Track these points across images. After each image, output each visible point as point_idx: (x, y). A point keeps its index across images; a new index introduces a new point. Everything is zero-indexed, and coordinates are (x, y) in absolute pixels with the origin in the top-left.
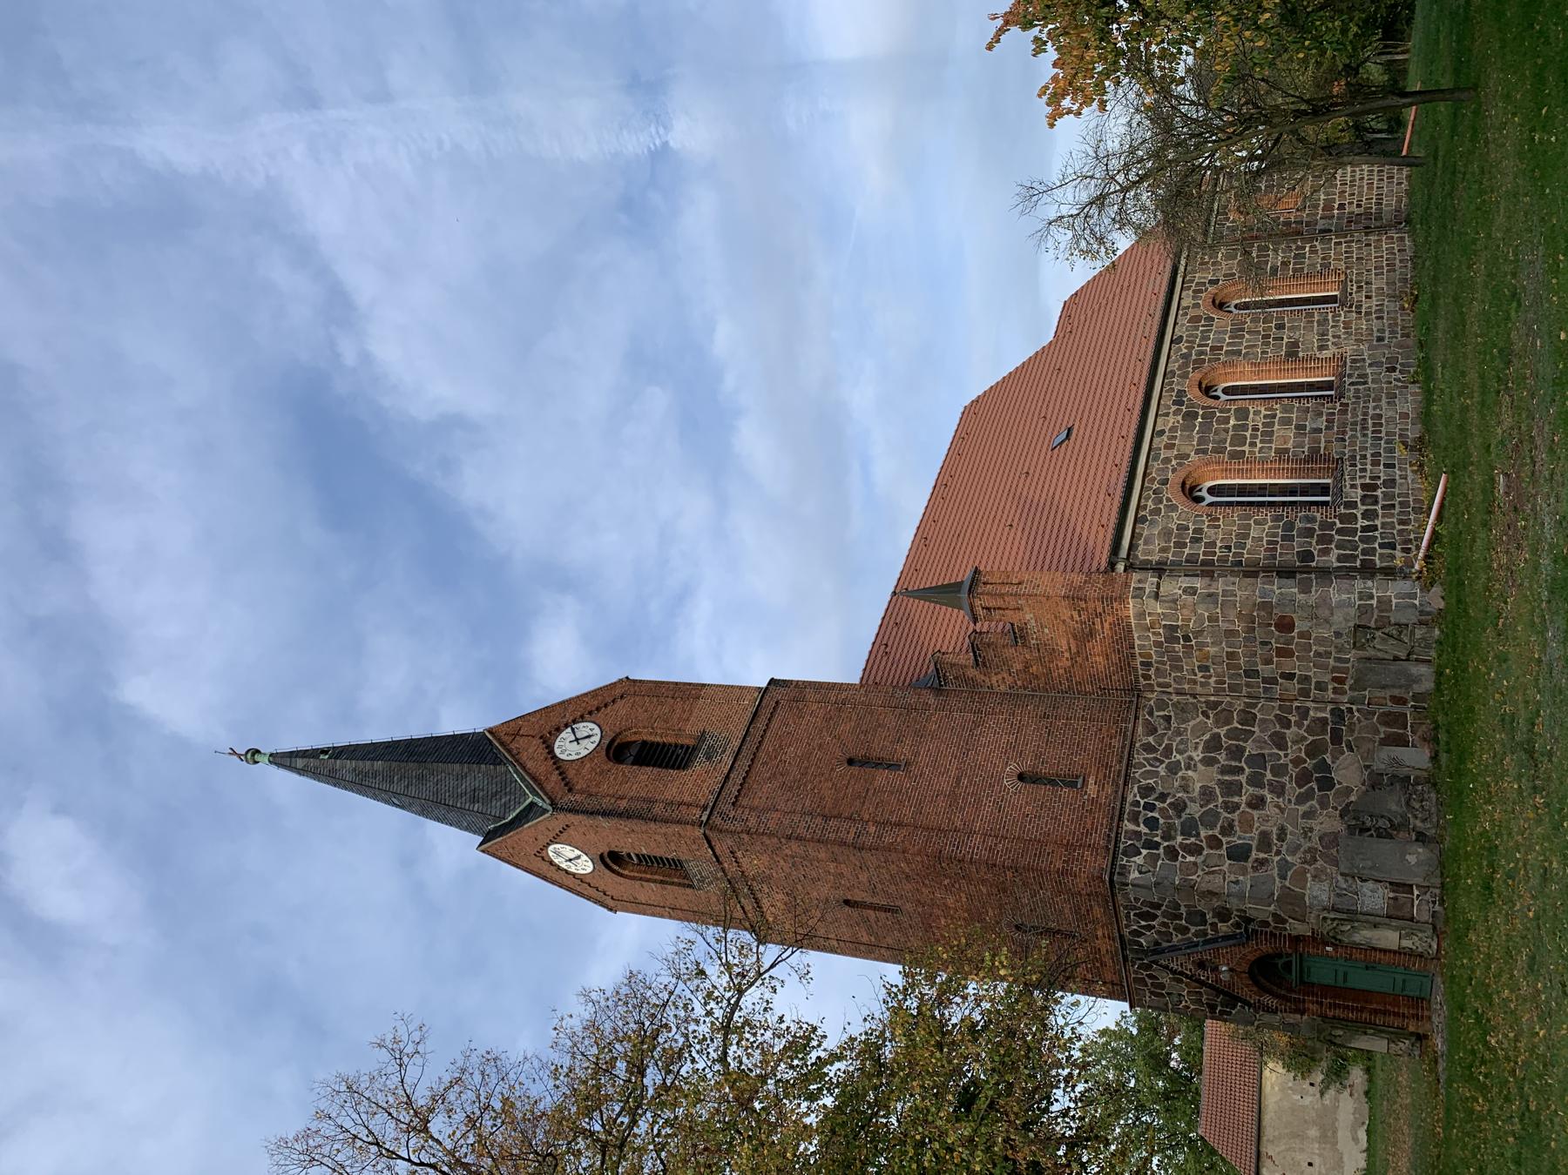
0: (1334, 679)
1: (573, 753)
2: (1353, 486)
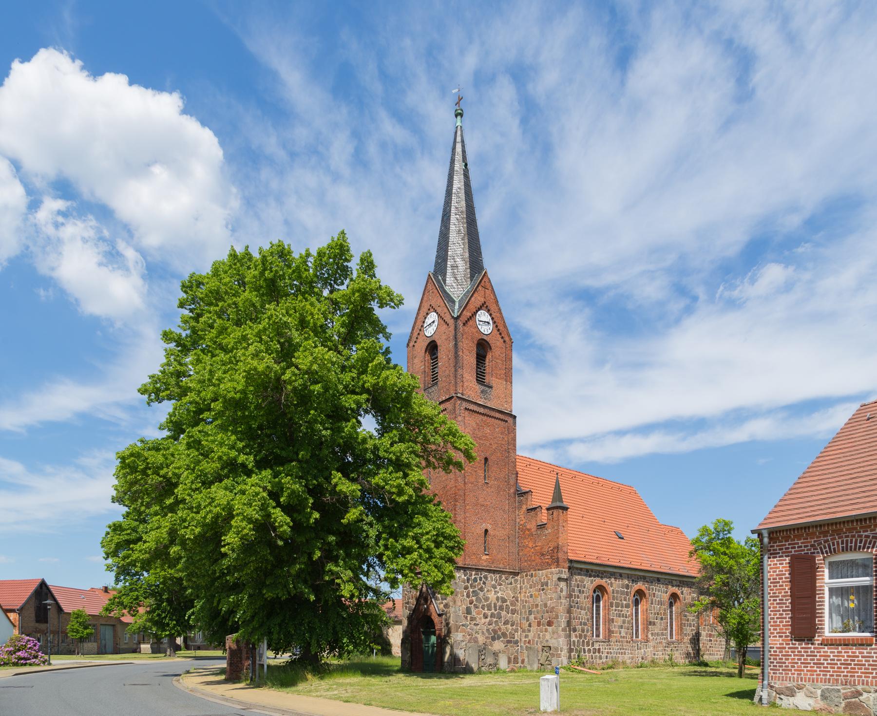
0: (530, 641)
2: (600, 645)
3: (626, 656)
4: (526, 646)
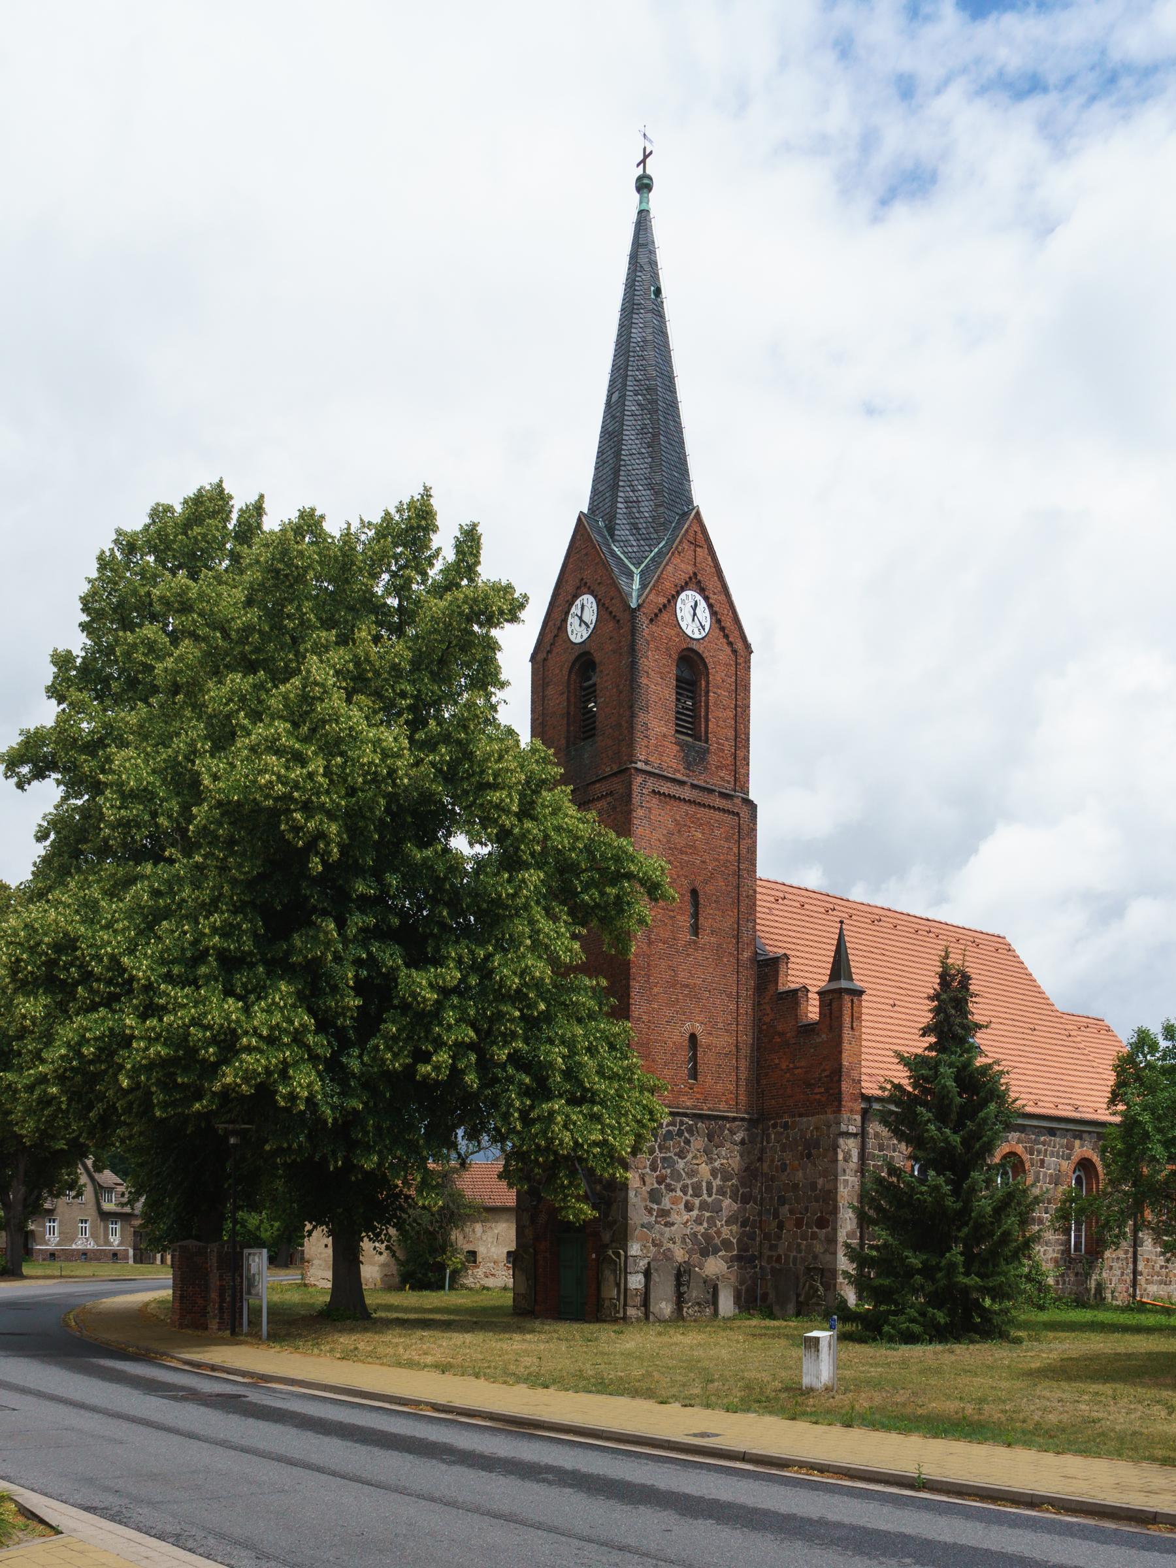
1: (682, 614)
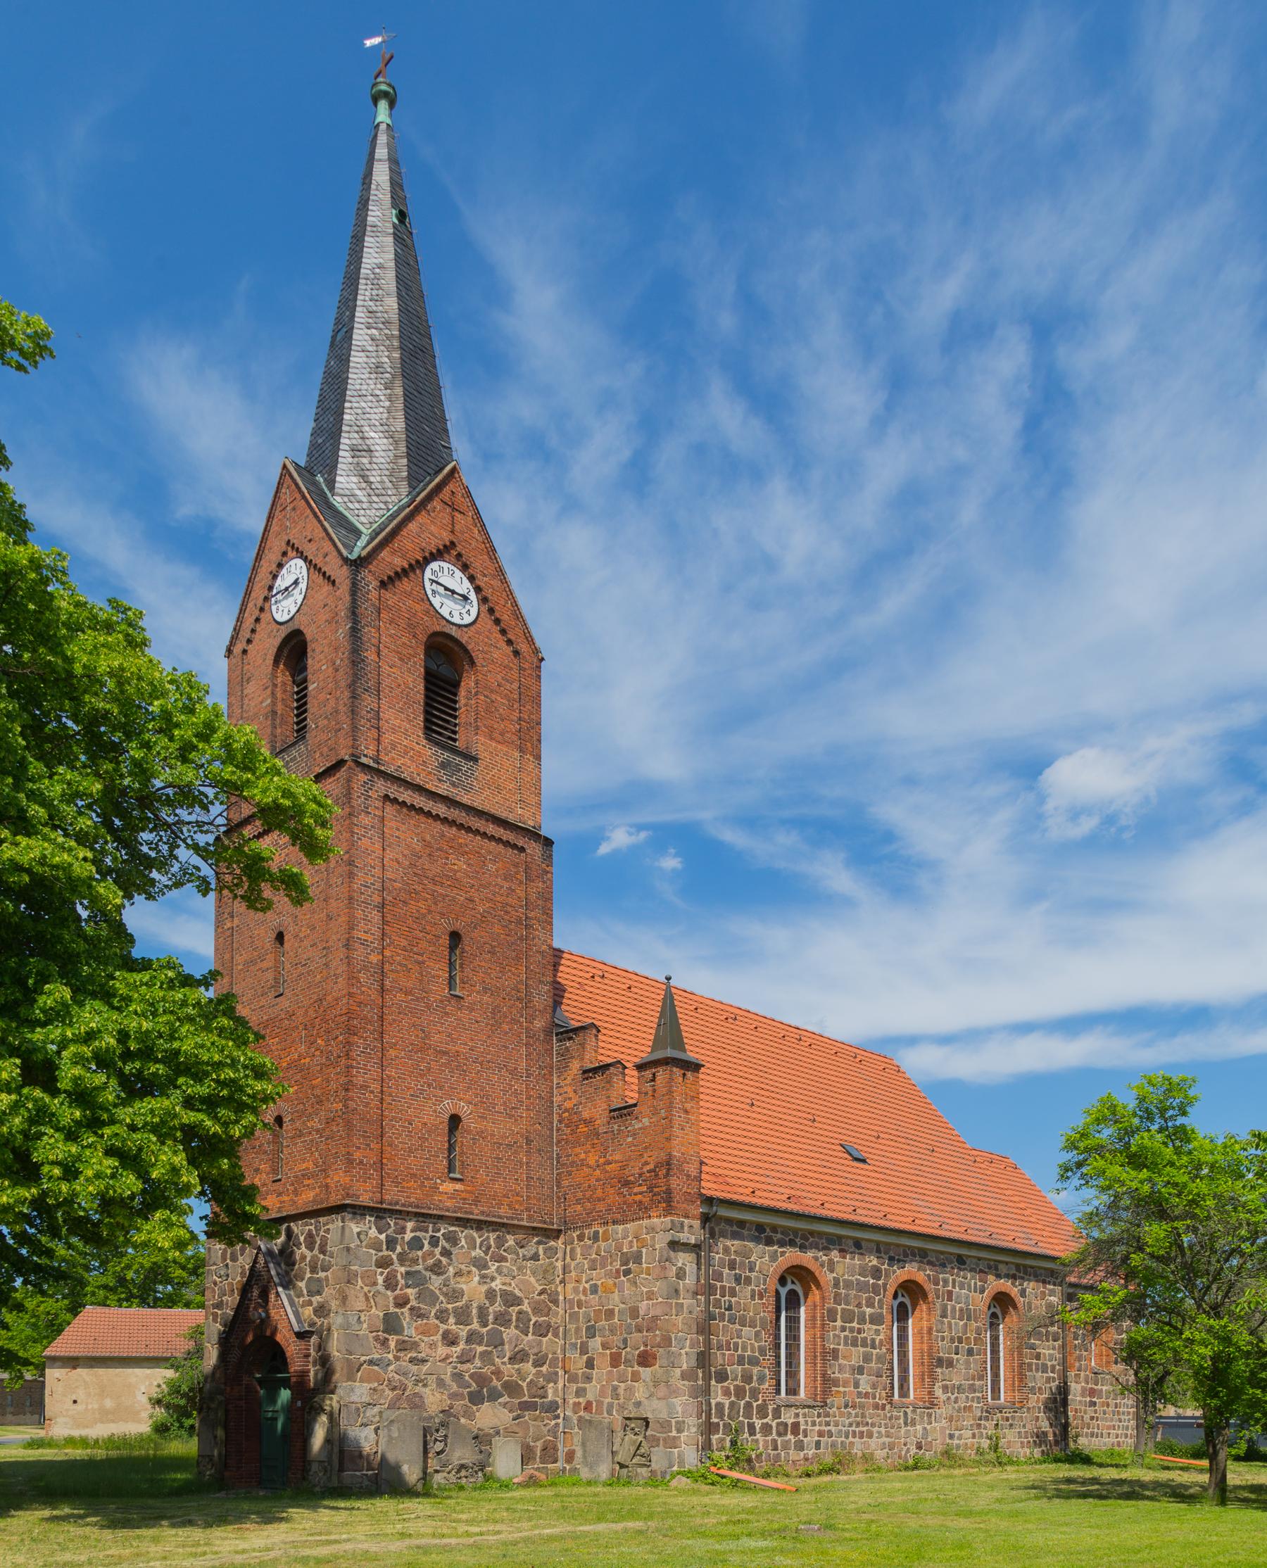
0: (589, 1404)
2: (797, 1415)
3: (873, 1442)
4: (580, 1419)
